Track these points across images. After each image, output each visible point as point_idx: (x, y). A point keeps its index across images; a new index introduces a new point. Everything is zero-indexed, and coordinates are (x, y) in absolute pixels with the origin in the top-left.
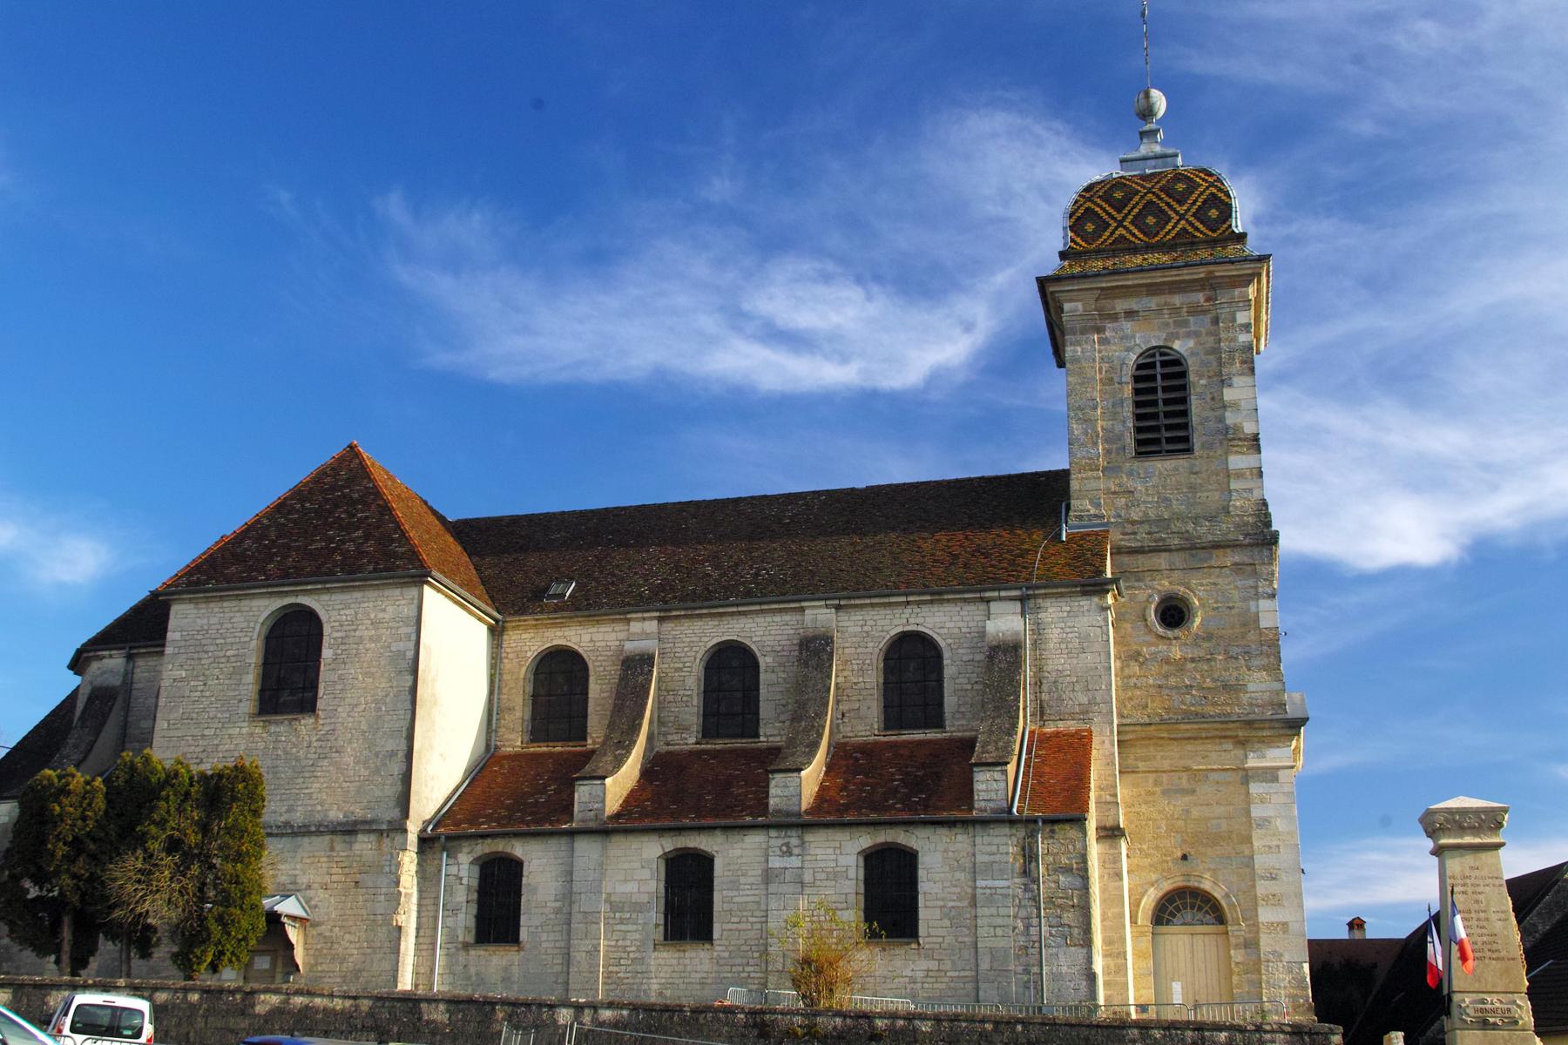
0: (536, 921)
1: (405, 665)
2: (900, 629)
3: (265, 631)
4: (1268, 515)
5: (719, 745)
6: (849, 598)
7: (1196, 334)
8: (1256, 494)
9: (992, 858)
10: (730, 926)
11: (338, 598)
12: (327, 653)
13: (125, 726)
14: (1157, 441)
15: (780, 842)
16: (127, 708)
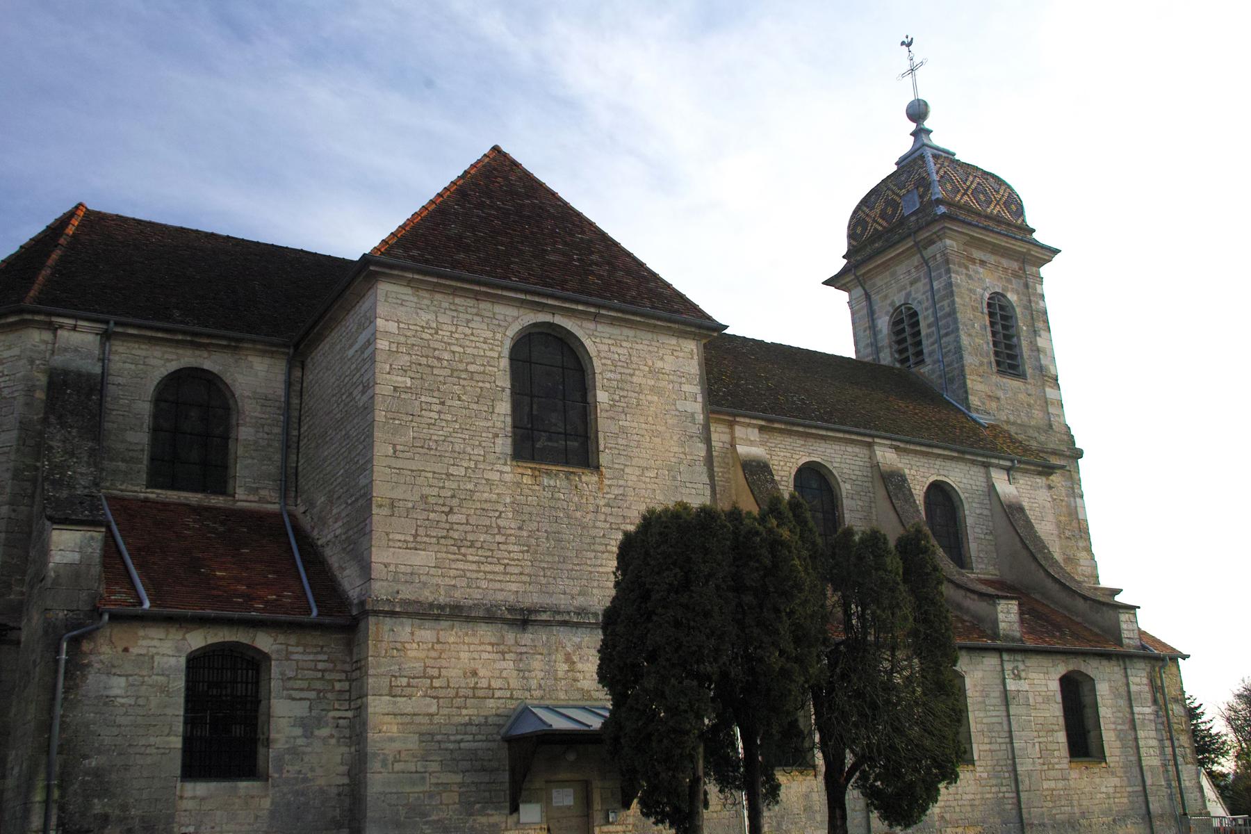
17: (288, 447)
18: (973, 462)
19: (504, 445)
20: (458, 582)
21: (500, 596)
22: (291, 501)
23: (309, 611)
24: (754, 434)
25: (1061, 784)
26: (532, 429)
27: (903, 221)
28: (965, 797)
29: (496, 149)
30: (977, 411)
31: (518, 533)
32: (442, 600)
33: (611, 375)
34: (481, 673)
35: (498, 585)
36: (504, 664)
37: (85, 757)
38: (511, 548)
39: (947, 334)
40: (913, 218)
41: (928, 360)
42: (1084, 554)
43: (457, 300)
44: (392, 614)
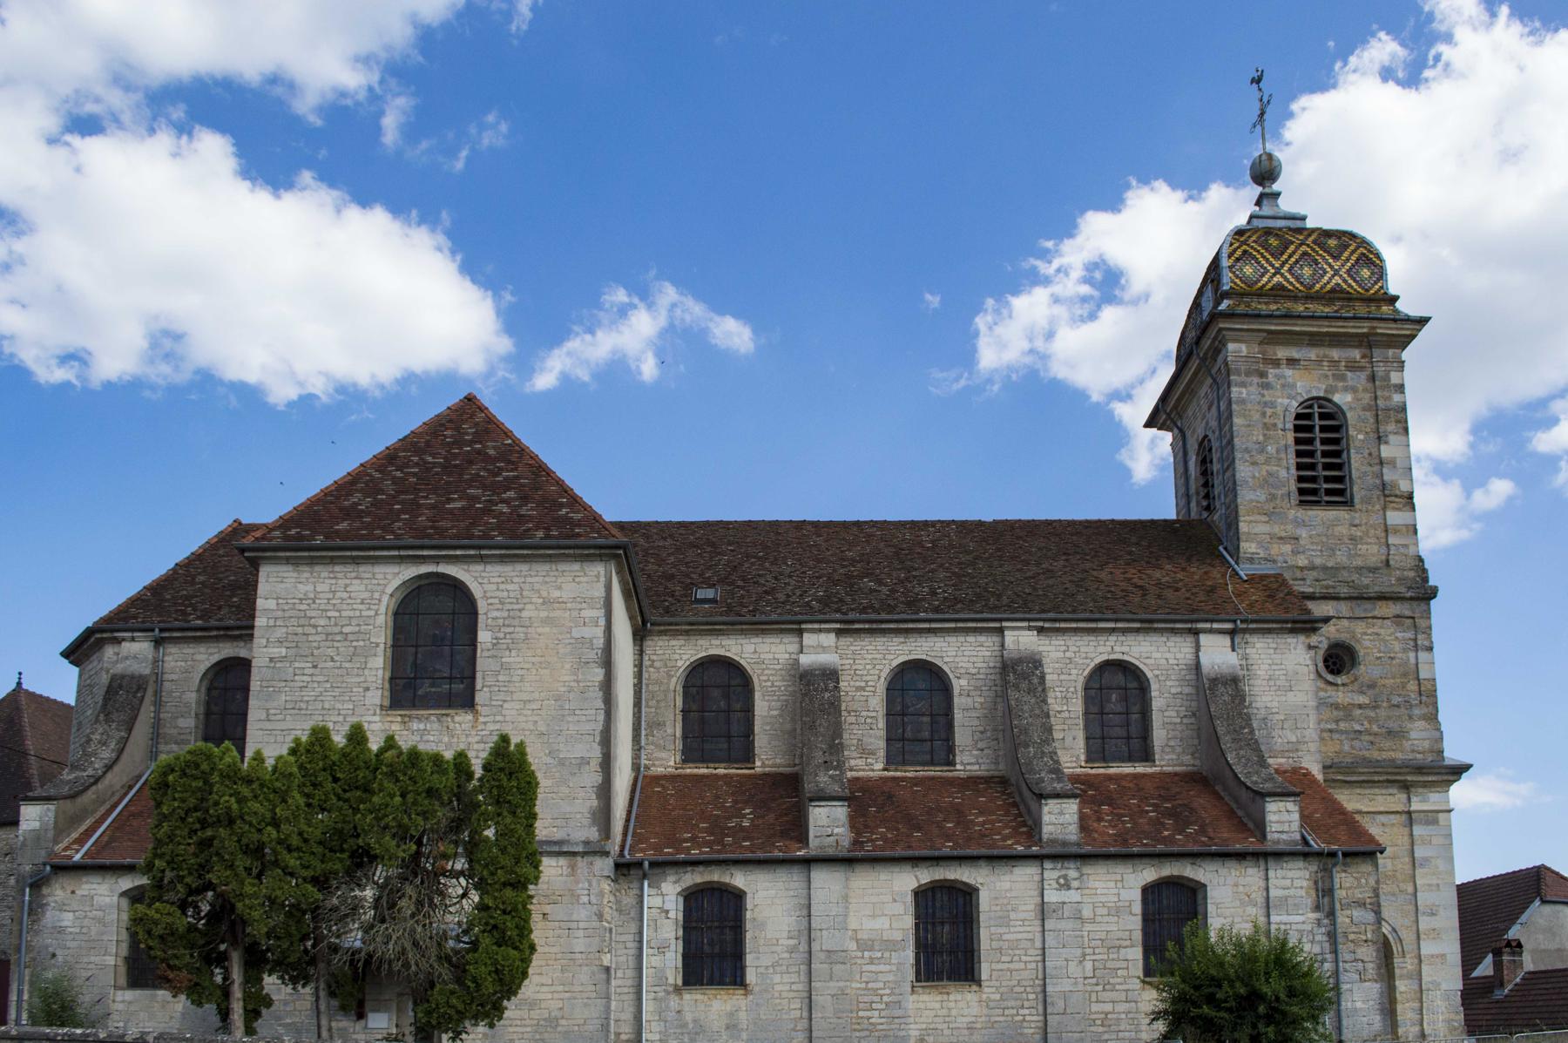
0: (766, 960)
1: (593, 655)
2: (1105, 657)
3: (393, 606)
4: (1425, 571)
5: (910, 773)
6: (1055, 620)
7: (1354, 390)
8: (1412, 551)
9: (1286, 892)
10: (1000, 966)
11: (494, 571)
12: (484, 636)
13: (157, 724)
14: (1314, 492)
15: (1056, 874)
16: (158, 703)
18: (1173, 631)
24: (829, 639)
26: (415, 678)
28: (960, 1019)
42: (1421, 724)
43: (337, 568)
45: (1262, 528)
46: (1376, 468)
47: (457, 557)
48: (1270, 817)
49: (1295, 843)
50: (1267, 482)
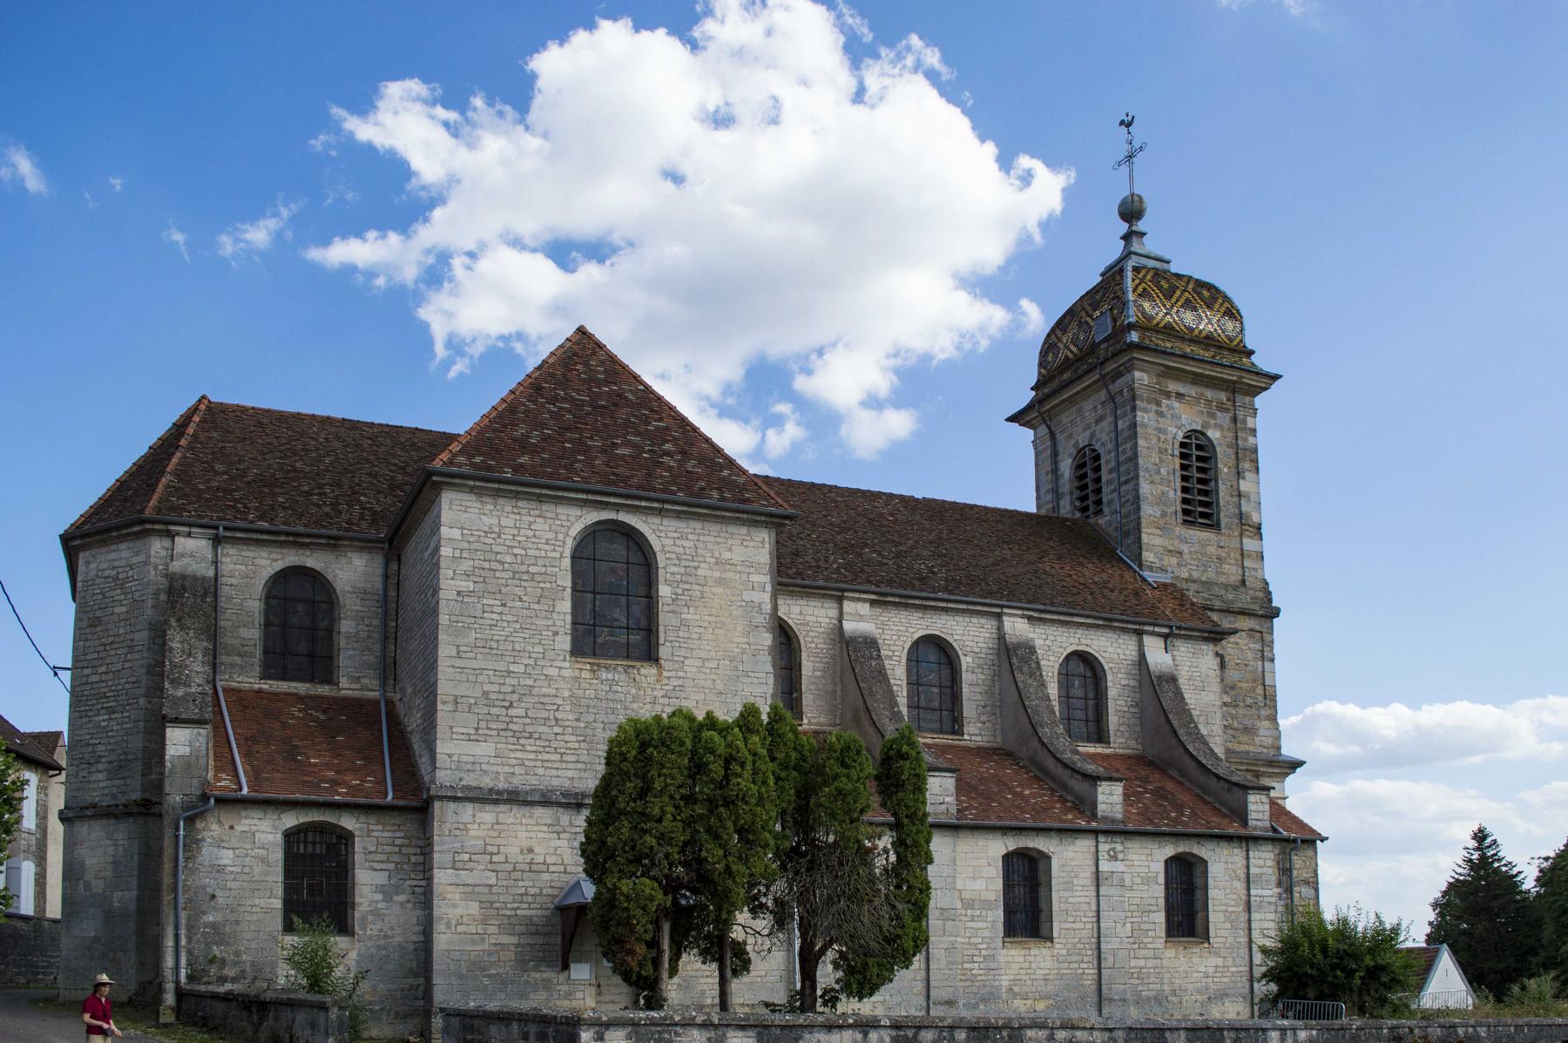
2: (1074, 648)
7: (1221, 428)
11: (671, 525)
12: (664, 591)
17: (386, 638)
18: (1123, 630)
19: (564, 642)
20: (517, 770)
21: (555, 782)
22: (389, 689)
23: (386, 794)
24: (864, 608)
25: (1151, 963)
27: (1094, 346)
29: (581, 331)
30: (1151, 569)
31: (575, 724)
32: (501, 786)
33: (675, 569)
34: (537, 850)
35: (554, 772)
36: (558, 843)
37: (204, 913)
38: (567, 738)
39: (1126, 482)
40: (1104, 346)
41: (1106, 510)
42: (1267, 723)
43: (520, 504)
44: (455, 799)
45: (1158, 541)
46: (1236, 499)
47: (608, 503)
48: (1251, 807)
49: (1265, 829)
50: (1161, 500)
